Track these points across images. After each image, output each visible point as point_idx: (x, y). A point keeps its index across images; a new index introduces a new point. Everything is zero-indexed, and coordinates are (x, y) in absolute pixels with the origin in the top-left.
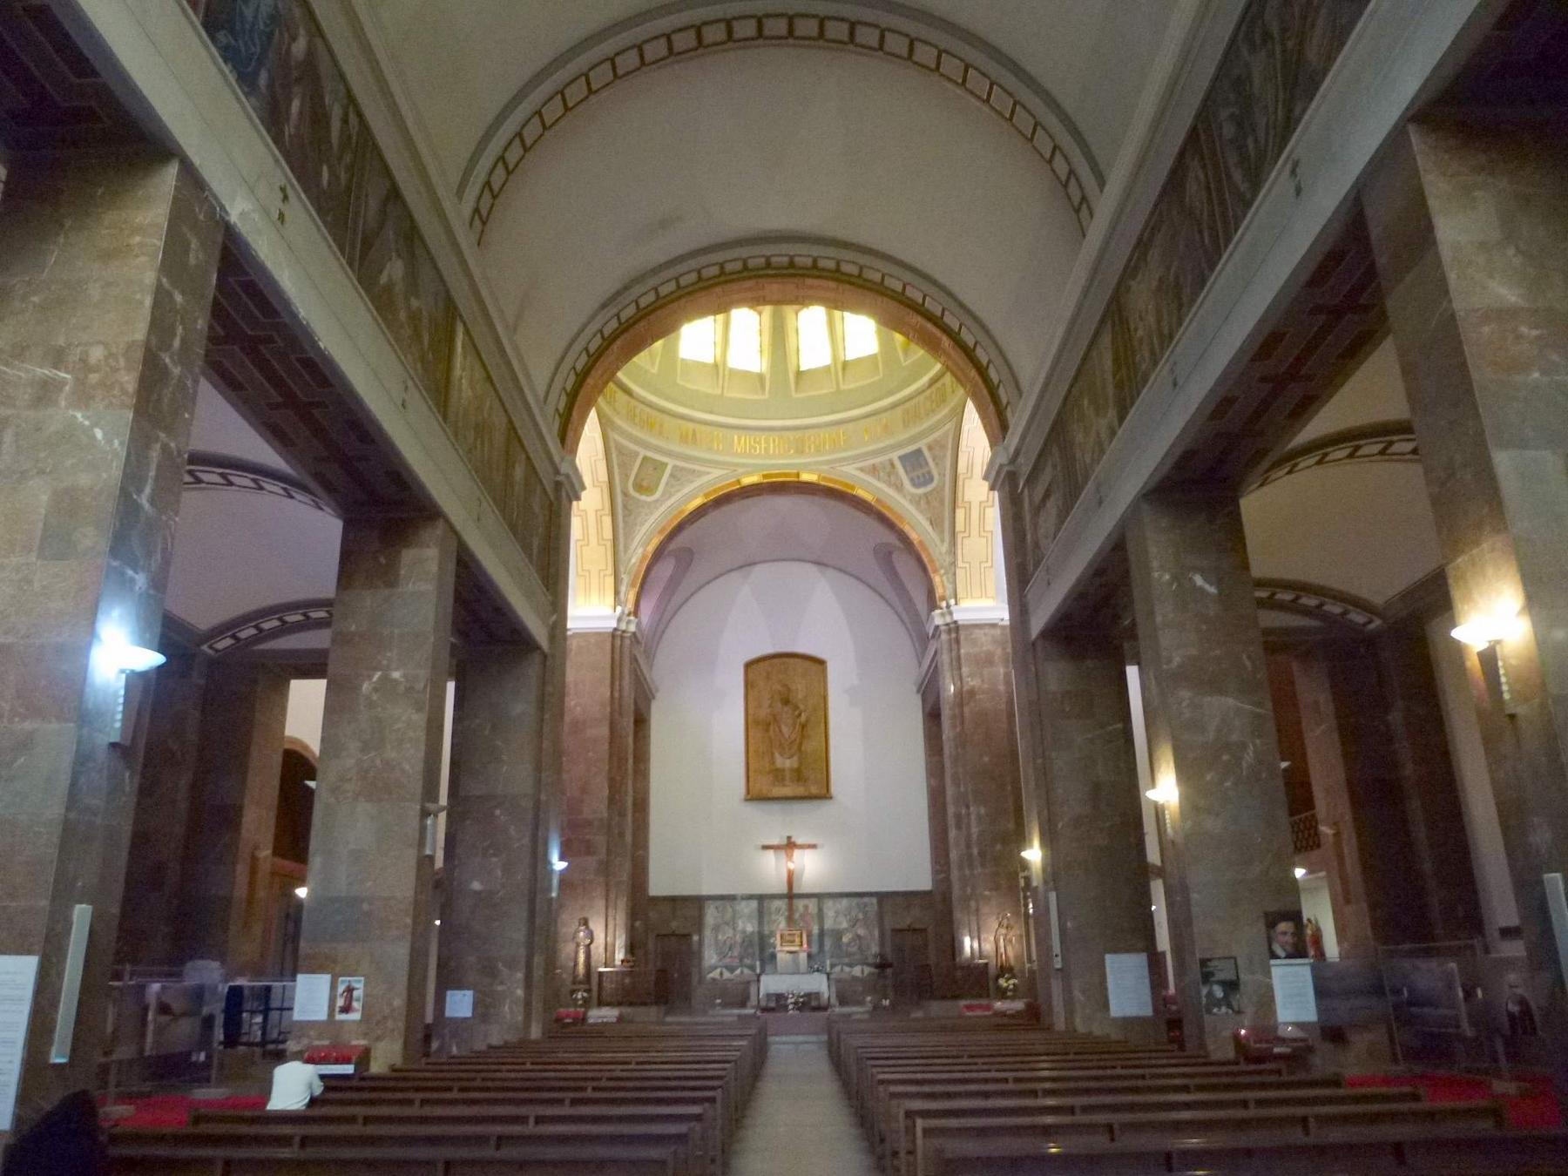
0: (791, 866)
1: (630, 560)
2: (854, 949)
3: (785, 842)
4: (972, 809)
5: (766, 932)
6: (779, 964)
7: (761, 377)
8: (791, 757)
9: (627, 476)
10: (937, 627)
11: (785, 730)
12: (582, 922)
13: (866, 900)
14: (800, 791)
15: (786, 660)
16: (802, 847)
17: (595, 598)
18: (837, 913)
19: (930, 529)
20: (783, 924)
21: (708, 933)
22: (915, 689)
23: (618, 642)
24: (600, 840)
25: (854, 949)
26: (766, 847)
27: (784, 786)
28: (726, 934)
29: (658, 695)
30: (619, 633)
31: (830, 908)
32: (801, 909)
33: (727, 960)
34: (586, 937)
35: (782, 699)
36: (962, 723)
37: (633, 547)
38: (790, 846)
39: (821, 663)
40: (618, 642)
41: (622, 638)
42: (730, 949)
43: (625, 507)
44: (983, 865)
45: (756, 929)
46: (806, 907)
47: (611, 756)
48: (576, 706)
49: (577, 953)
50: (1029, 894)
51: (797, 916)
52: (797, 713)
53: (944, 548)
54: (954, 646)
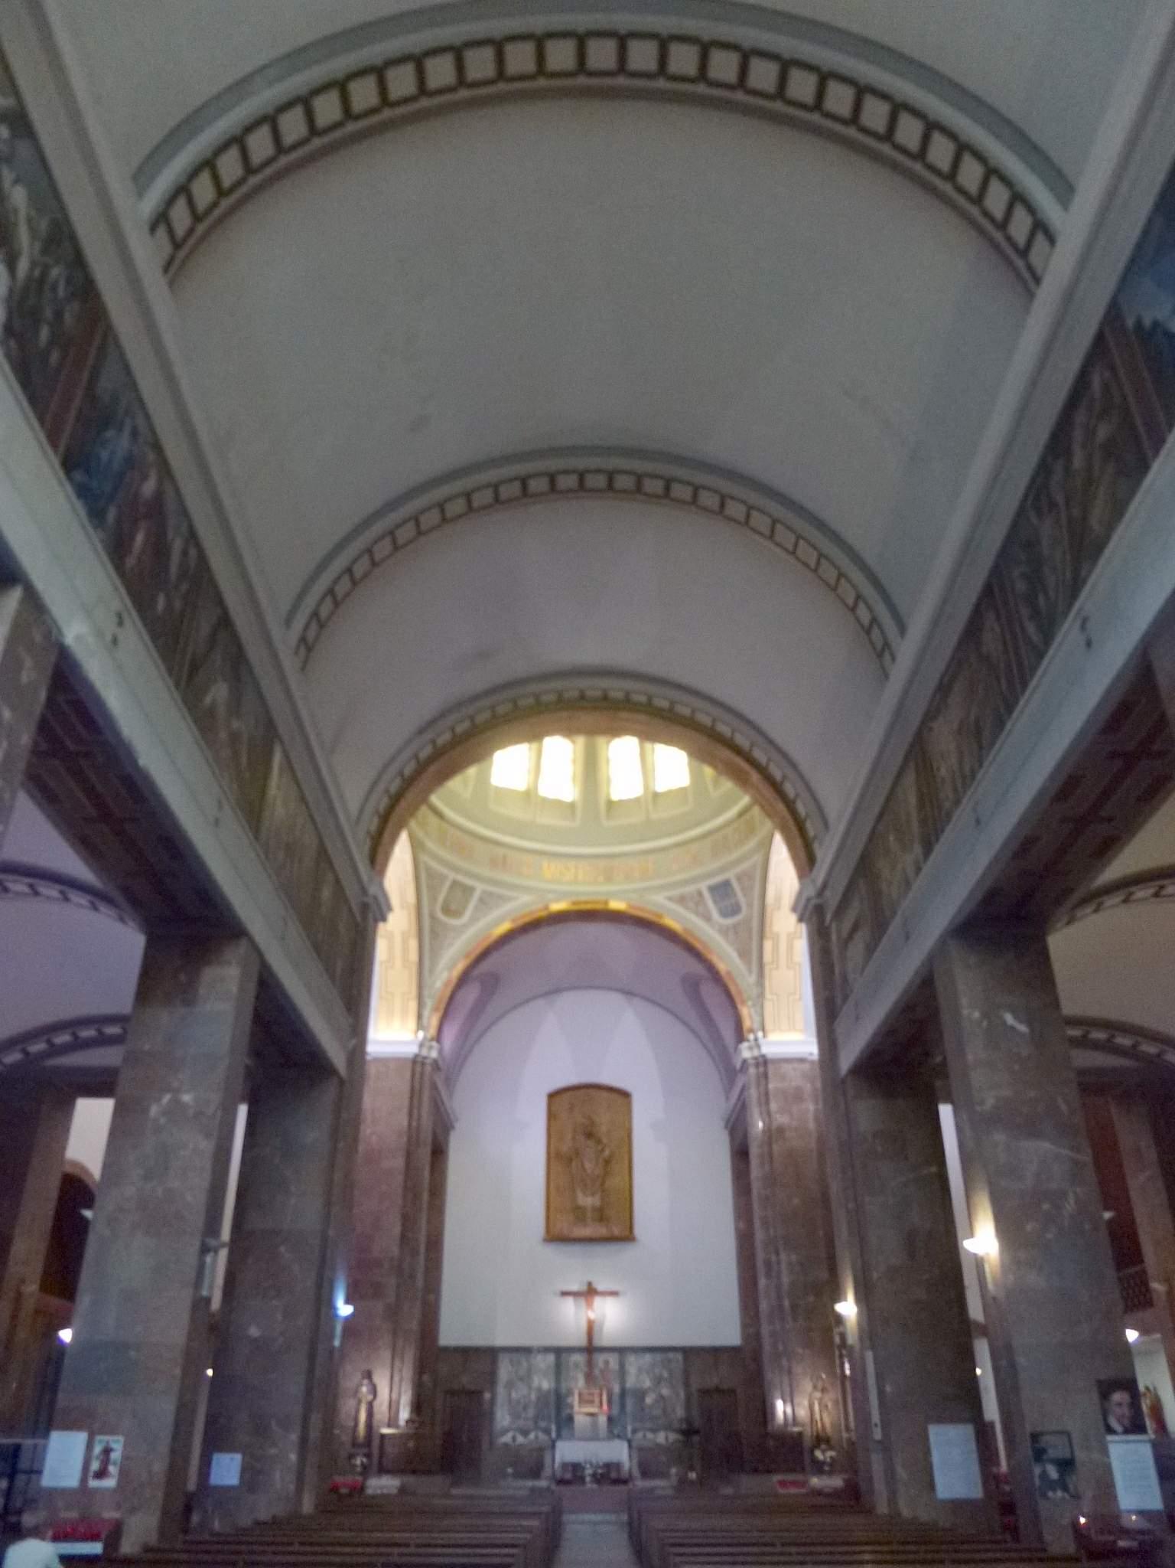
0: (592, 1315)
2: (657, 1412)
3: (584, 1288)
4: (783, 1256)
5: (564, 1391)
7: (572, 806)
11: (588, 1165)
13: (671, 1355)
14: (603, 1231)
18: (640, 1370)
21: (501, 1391)
22: (722, 1124)
25: (657, 1412)
26: (565, 1294)
29: (457, 1125)
33: (521, 1423)
38: (590, 1292)
39: (625, 1095)
44: (795, 1320)
45: (553, 1385)
46: (607, 1363)
49: (357, 1411)
51: (597, 1372)
52: (600, 1148)
53: (752, 979)
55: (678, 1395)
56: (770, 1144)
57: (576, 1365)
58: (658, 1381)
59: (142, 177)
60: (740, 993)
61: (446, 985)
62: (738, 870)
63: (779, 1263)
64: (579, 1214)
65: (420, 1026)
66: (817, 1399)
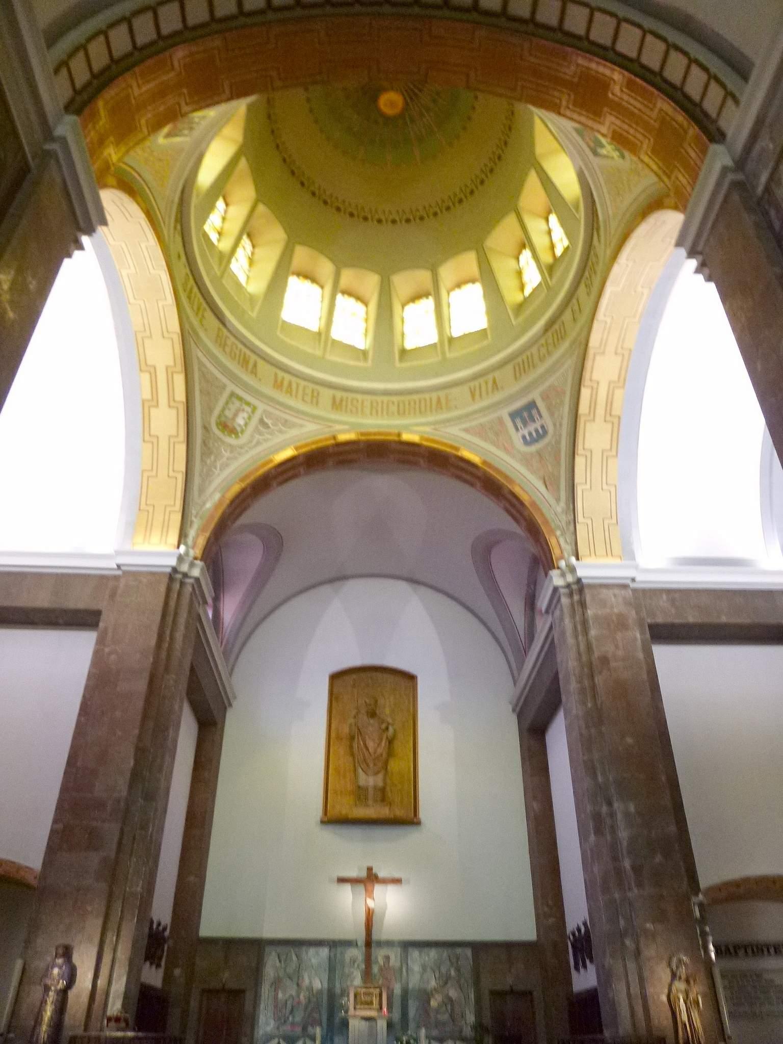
0: (371, 903)
1: (204, 503)
2: (445, 1017)
3: (364, 874)
4: (616, 805)
5: (338, 991)
6: (350, 1035)
7: (364, 353)
8: (376, 773)
9: (211, 410)
10: (556, 589)
11: (371, 745)
12: (61, 951)
13: (459, 951)
14: (384, 812)
15: (374, 674)
16: (385, 881)
17: (155, 538)
18: (424, 968)
19: (542, 489)
20: (358, 981)
21: (266, 990)
22: (510, 708)
23: (176, 586)
24: (111, 830)
25: (445, 1017)
26: (342, 880)
27: (367, 805)
28: (288, 992)
29: (234, 703)
30: (179, 576)
31: (416, 958)
32: (381, 961)
33: (287, 1028)
34: (61, 976)
35: (367, 713)
36: (594, 697)
37: (211, 488)
38: (370, 879)
39: (411, 678)
40: (176, 586)
41: (182, 584)
42: (292, 1012)
43: (204, 443)
44: (640, 885)
45: (326, 985)
46: (387, 958)
47: (145, 717)
48: (110, 654)
49: (43, 1002)
50: (707, 929)
51: (375, 969)
52: (384, 726)
53: (560, 507)
54: (578, 609)
55: (467, 998)
56: (592, 677)
57: (353, 961)
58: (445, 981)
59: (52, 37)
60: (546, 522)
61: (216, 507)
62: (542, 388)
63: (612, 815)
64: (360, 795)
65: (182, 536)
66: (681, 991)
